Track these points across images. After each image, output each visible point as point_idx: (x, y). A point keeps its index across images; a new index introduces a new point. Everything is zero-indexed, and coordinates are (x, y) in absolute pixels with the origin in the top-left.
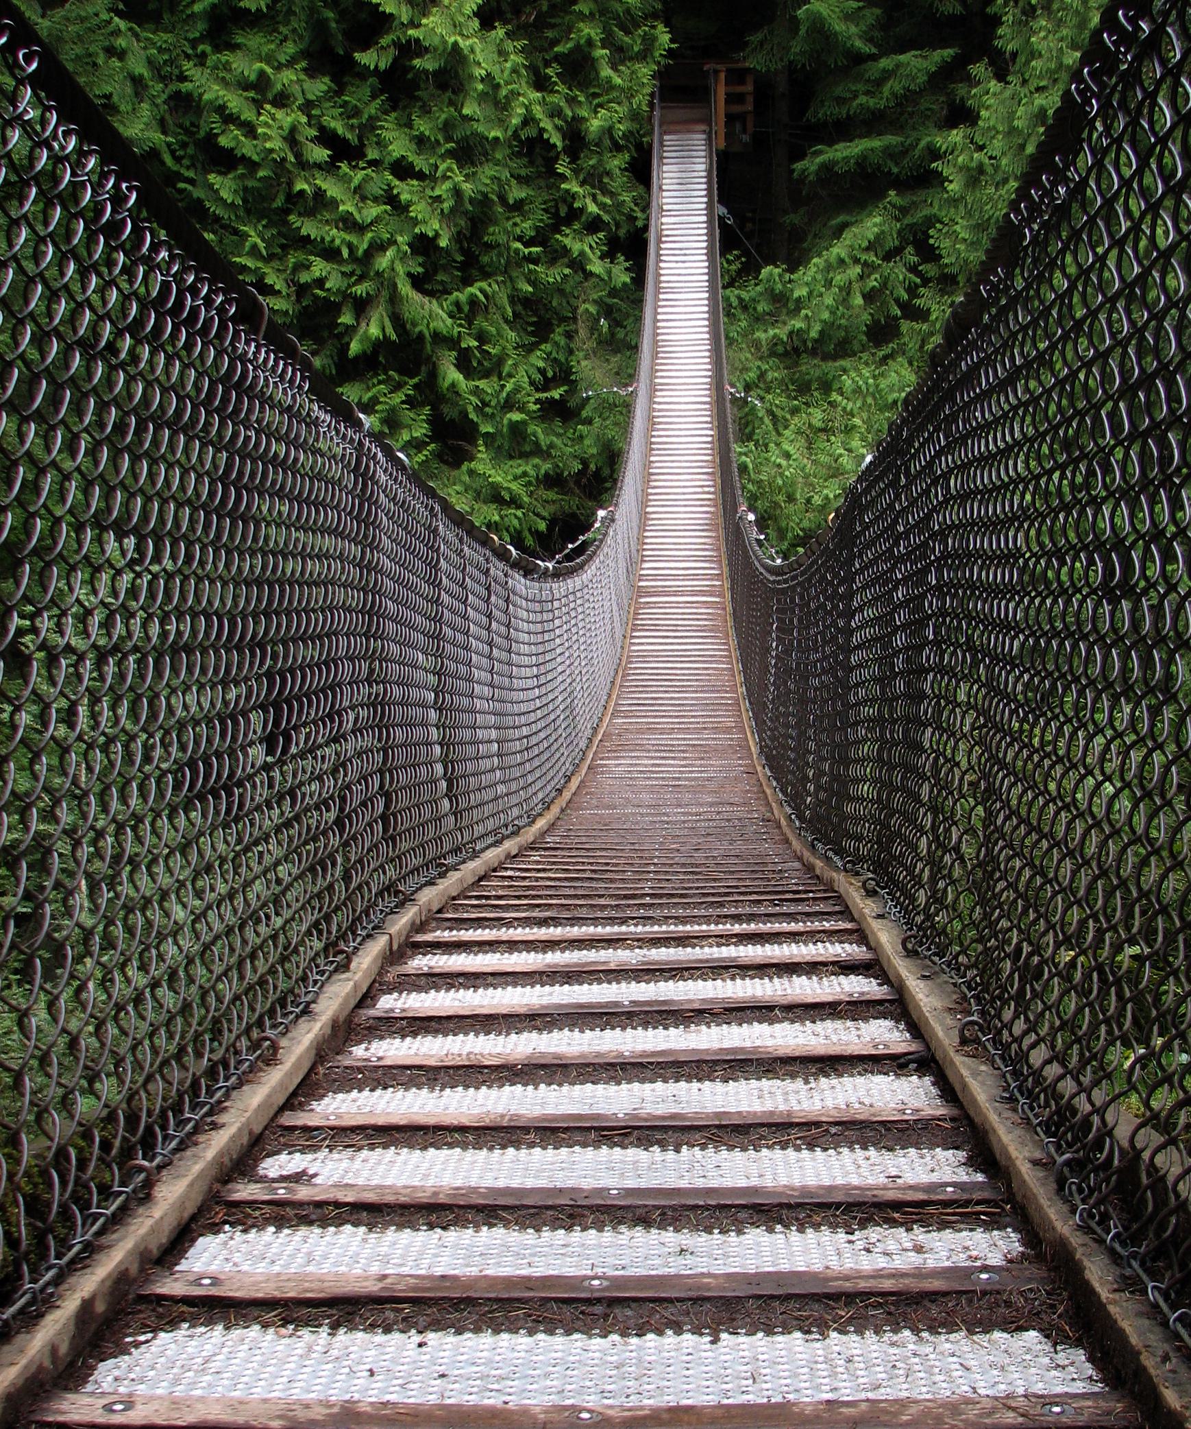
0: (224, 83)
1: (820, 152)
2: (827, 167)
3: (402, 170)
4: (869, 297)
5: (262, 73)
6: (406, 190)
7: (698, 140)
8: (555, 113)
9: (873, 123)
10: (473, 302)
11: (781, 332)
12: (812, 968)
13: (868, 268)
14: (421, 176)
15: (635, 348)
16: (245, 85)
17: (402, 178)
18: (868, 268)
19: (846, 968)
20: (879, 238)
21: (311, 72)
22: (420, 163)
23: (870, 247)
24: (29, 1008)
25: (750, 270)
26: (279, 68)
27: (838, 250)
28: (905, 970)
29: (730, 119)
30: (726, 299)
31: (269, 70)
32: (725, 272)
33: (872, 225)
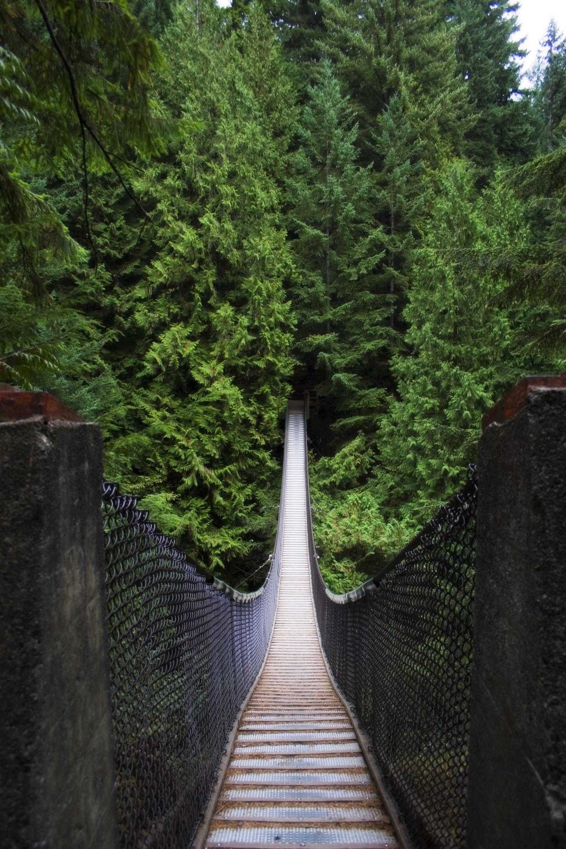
0: (146, 402)
1: (341, 421)
2: (343, 426)
3: (203, 431)
4: (357, 466)
5: (158, 399)
6: (204, 437)
7: (301, 417)
8: (253, 413)
9: (359, 412)
10: (226, 472)
11: (327, 482)
12: (328, 730)
13: (356, 457)
14: (209, 433)
15: (280, 488)
16: (152, 402)
17: (203, 434)
18: (356, 457)
19: (342, 714)
20: (359, 447)
21: (174, 399)
22: (209, 429)
23: (356, 450)
24: (142, 118)
25: (317, 458)
26: (163, 397)
27: (346, 450)
28: (358, 731)
29: (311, 407)
30: (310, 469)
31: (160, 398)
32: (309, 459)
33: (357, 442)
